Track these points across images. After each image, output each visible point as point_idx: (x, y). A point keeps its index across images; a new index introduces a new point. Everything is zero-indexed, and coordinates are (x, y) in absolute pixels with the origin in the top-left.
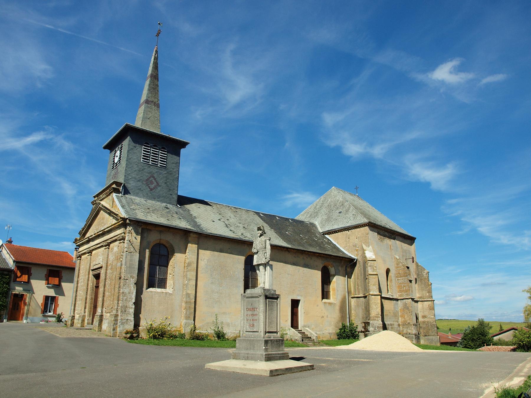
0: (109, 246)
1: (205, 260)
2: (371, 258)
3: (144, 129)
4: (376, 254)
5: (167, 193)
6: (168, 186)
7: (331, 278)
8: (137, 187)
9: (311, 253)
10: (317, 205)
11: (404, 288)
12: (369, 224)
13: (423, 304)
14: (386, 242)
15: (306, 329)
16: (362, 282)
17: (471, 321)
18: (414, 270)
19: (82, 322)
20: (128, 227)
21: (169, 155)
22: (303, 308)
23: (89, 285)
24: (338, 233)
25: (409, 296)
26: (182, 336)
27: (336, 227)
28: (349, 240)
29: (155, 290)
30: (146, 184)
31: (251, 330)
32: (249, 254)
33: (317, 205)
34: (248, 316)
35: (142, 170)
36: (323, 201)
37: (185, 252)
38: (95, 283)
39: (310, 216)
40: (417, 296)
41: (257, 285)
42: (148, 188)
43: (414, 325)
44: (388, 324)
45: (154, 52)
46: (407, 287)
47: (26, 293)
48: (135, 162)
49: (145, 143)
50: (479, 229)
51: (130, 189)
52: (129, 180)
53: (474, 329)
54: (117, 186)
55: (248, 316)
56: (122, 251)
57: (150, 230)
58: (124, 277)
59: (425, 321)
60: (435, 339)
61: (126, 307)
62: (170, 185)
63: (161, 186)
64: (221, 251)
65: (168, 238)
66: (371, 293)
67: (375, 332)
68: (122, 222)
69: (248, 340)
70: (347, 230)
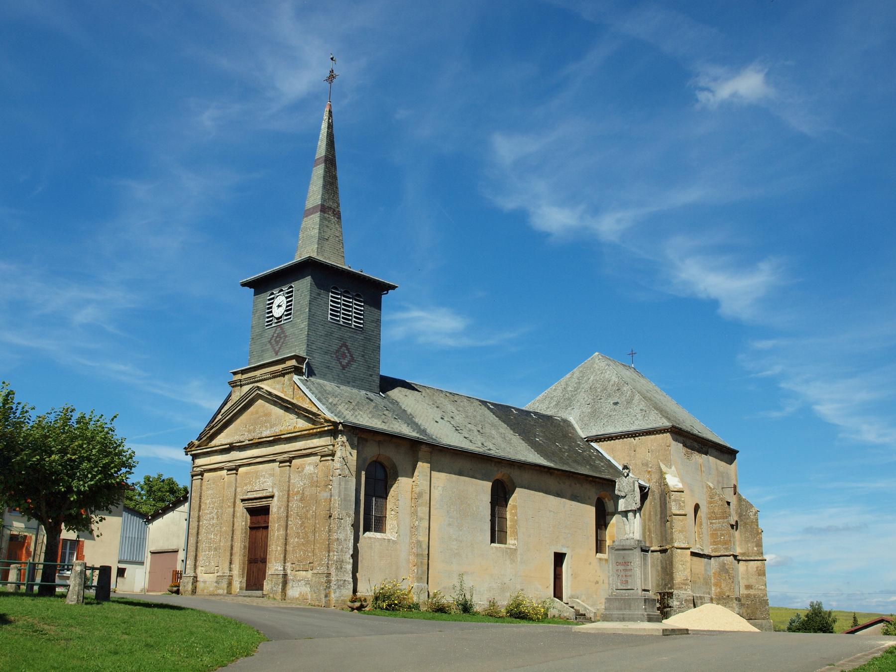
0: (291, 463)
1: (440, 488)
2: (676, 487)
3: (333, 265)
4: (682, 480)
5: (365, 373)
6: (366, 361)
7: (608, 517)
8: (325, 364)
9: (559, 473)
10: (567, 385)
11: (721, 538)
12: (673, 429)
13: (747, 566)
14: (694, 459)
15: (577, 601)
16: (658, 527)
17: (790, 609)
18: (735, 508)
19: (228, 587)
20: (340, 435)
21: (367, 307)
22: (571, 568)
23: (236, 525)
24: (614, 440)
25: (730, 551)
26: (416, 606)
27: (610, 430)
28: (635, 454)
29: (373, 534)
30: (336, 359)
31: (624, 588)
32: (496, 479)
33: (567, 385)
34: (619, 571)
35: (329, 334)
36: (578, 379)
37: (412, 476)
38: (249, 521)
39: (556, 405)
40: (738, 551)
41: (506, 528)
42: (339, 365)
43: (736, 600)
44: (697, 597)
45: (326, 117)
46: (727, 536)
47: (31, 534)
48: (320, 321)
49: (333, 288)
50: (817, 408)
51: (315, 366)
52: (313, 353)
53: (808, 620)
54: (298, 364)
55: (619, 571)
56: (331, 474)
57: (366, 441)
58: (339, 515)
59: (749, 594)
60: (765, 626)
61: (342, 561)
62: (369, 360)
63: (357, 362)
64: (460, 473)
65: (390, 453)
66: (676, 545)
67: (681, 610)
68: (330, 428)
69: (621, 598)
70: (632, 437)
